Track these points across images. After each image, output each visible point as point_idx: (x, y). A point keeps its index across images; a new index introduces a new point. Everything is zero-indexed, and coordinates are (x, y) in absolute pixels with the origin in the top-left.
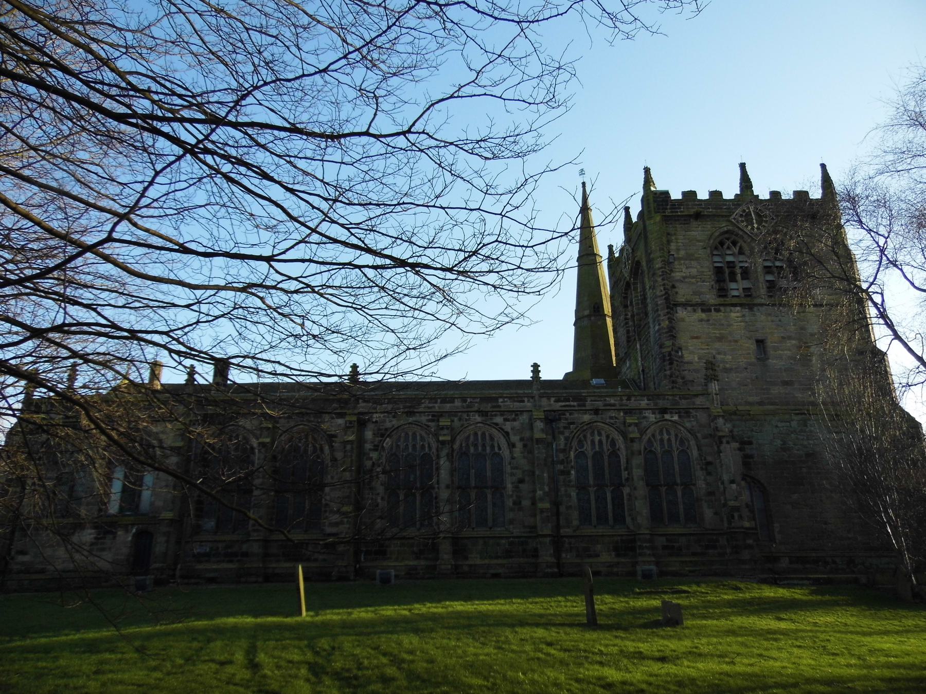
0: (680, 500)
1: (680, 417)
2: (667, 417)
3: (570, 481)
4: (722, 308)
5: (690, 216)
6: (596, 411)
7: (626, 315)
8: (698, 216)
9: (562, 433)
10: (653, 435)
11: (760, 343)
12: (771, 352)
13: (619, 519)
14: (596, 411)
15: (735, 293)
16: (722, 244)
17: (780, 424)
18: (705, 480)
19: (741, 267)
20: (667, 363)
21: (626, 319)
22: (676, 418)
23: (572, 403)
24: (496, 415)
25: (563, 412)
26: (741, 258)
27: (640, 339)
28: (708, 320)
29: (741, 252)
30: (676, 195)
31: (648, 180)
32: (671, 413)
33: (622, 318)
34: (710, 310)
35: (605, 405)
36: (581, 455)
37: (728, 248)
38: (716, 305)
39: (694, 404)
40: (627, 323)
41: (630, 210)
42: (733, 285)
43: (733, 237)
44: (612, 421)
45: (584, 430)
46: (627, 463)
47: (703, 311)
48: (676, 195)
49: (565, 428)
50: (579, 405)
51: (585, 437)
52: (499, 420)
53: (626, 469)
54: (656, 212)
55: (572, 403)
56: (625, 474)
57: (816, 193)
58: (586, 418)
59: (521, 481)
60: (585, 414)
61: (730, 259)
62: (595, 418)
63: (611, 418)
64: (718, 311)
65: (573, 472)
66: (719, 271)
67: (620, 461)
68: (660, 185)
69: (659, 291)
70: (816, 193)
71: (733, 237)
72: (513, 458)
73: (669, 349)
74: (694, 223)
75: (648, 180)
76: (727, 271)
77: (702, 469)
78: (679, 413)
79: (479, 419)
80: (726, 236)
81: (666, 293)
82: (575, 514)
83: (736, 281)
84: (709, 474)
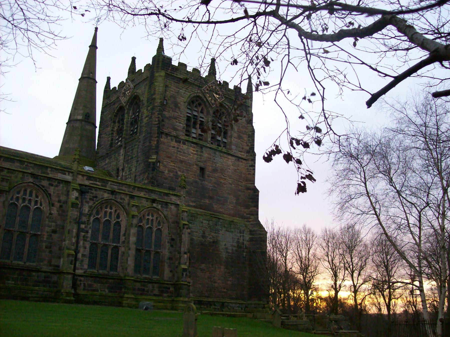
0: (152, 261)
1: (162, 207)
2: (155, 205)
3: (87, 237)
4: (186, 143)
5: (181, 79)
6: (113, 192)
7: (113, 128)
8: (185, 81)
9: (87, 202)
10: (144, 216)
11: (202, 170)
12: (206, 177)
13: (114, 267)
14: (113, 192)
15: (194, 135)
16: (193, 102)
17: (204, 222)
18: (169, 249)
19: (200, 121)
20: (151, 169)
21: (112, 131)
22: (159, 207)
23: (98, 183)
24: (44, 180)
25: (91, 188)
26: (202, 115)
27: (125, 147)
28: (178, 148)
29: (202, 112)
30: (175, 63)
31: (161, 48)
32: (157, 203)
33: (109, 129)
34: (180, 142)
35: (119, 189)
36: (97, 220)
37: (196, 107)
38: (184, 140)
39: (171, 200)
40: (112, 134)
41: (136, 60)
42: (194, 131)
43: (200, 101)
44: (121, 201)
45: (103, 204)
46: (126, 231)
47: (176, 141)
48: (175, 63)
49: (90, 199)
50: (102, 186)
51: (101, 208)
52: (45, 183)
53: (124, 235)
54: (162, 69)
55: (98, 183)
56: (122, 238)
57: (204, 73)
58: (106, 195)
59: (54, 232)
60: (105, 192)
61: (196, 114)
62: (111, 197)
63: (121, 199)
64: (184, 144)
65: (90, 231)
66: (188, 119)
67: (120, 229)
68: (167, 53)
69: (155, 121)
70: (204, 73)
71: (200, 101)
72: (51, 214)
73: (154, 161)
74: (181, 85)
75: (161, 48)
76: (193, 120)
77: (168, 242)
78: (162, 204)
79: (31, 180)
80: (197, 99)
81: (159, 124)
82: (86, 261)
83: (196, 128)
84: (172, 246)
